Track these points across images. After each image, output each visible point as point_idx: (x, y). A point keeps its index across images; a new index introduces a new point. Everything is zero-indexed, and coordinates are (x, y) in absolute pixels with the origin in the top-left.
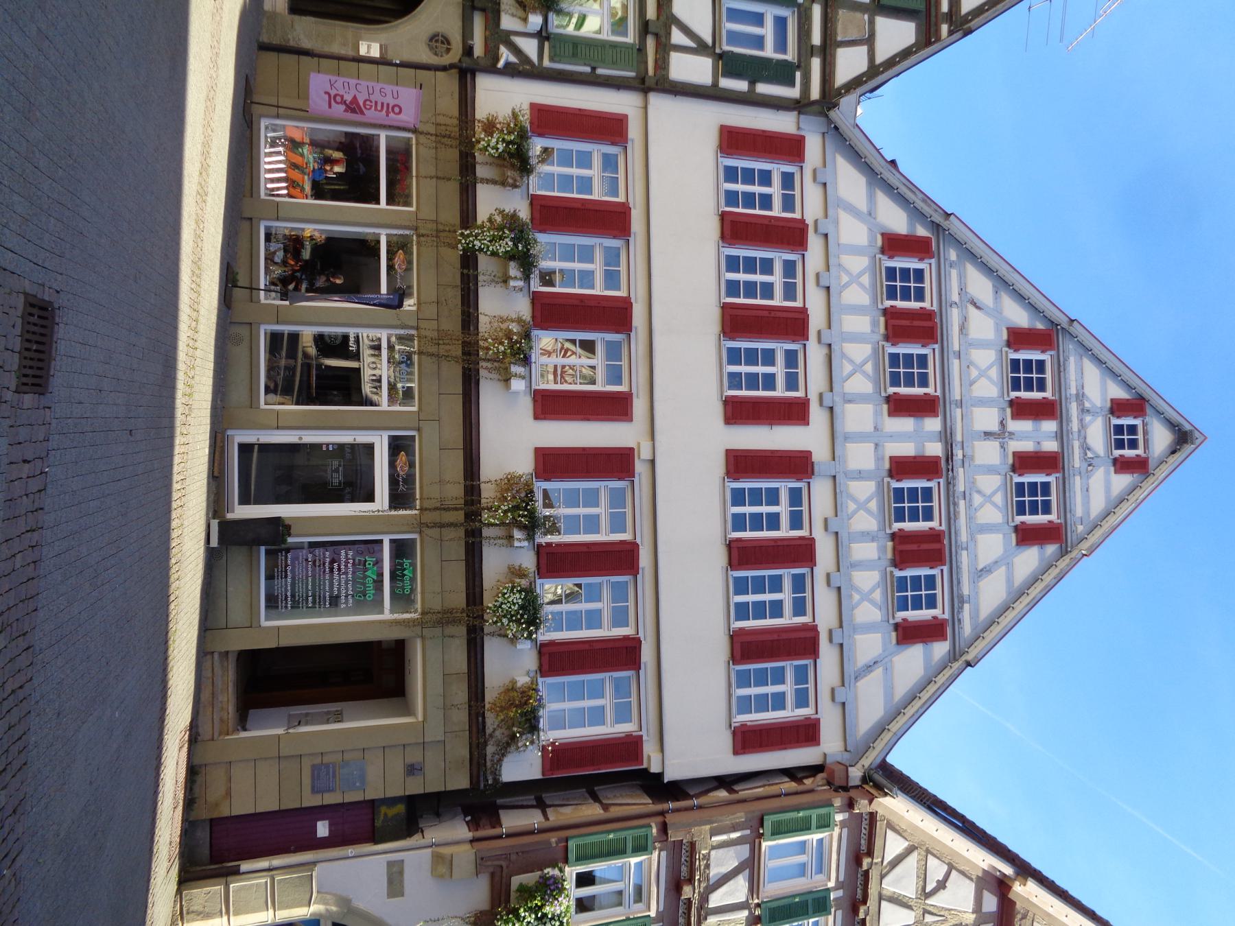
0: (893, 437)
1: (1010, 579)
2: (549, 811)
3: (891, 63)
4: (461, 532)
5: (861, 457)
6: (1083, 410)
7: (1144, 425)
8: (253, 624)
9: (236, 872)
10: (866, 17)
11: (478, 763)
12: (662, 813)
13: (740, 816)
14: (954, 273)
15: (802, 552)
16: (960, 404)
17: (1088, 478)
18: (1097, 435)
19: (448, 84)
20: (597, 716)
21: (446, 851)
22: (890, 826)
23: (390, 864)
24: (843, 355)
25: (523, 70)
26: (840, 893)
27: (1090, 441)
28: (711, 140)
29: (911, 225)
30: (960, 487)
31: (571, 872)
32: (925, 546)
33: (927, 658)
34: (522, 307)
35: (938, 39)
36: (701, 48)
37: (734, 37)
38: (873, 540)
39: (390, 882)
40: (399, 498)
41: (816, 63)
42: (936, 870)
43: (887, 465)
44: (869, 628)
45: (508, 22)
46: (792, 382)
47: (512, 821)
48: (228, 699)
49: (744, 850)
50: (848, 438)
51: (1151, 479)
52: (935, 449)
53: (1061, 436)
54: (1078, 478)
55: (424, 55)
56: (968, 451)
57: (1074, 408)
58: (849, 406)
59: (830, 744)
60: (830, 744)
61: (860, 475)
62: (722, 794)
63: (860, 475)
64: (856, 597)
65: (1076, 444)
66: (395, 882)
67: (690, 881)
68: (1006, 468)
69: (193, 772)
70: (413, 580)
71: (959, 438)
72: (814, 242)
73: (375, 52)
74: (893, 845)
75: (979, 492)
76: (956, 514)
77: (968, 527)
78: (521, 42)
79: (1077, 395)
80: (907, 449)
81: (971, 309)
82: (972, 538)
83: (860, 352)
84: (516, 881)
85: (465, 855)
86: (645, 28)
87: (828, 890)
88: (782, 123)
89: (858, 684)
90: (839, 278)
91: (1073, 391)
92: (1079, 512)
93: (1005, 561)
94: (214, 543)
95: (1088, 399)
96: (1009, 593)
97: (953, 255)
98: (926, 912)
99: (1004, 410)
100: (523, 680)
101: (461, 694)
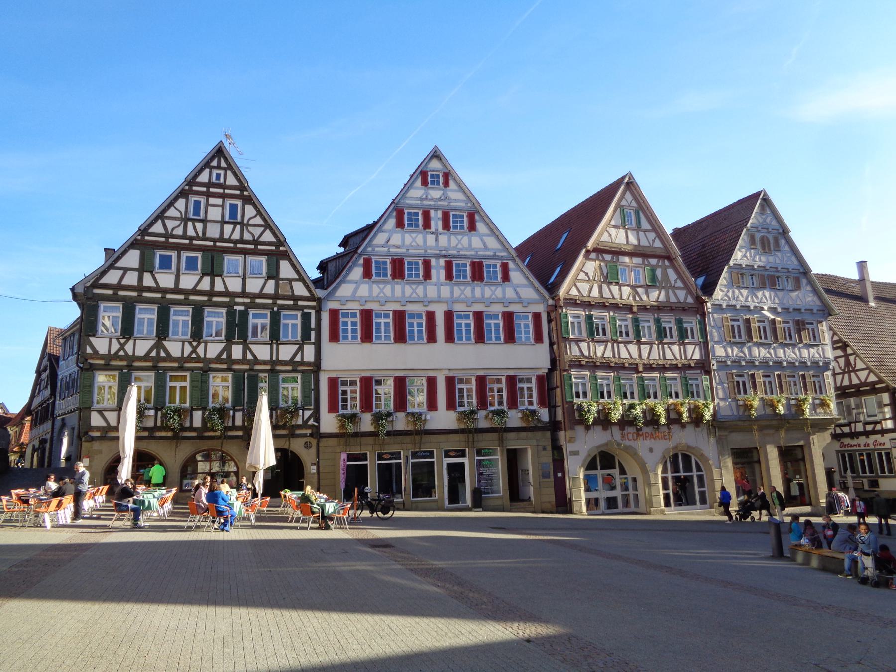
0: (438, 278)
1: (488, 236)
2: (557, 405)
3: (298, 272)
4: (475, 434)
5: (445, 291)
6: (426, 199)
7: (430, 171)
8: (502, 498)
9: (570, 499)
10: (280, 282)
11: (543, 428)
12: (560, 370)
13: (563, 345)
14: (377, 249)
15: (479, 316)
16: (426, 251)
17: (451, 199)
18: (435, 193)
19: (324, 442)
20: (527, 326)
21: (568, 438)
22: (568, 293)
23: (571, 455)
24: (410, 297)
25: (316, 415)
26: (587, 310)
27: (438, 197)
28: (334, 345)
29: (359, 266)
30: (455, 253)
31: (576, 400)
32: (477, 270)
33: (514, 270)
34: (401, 415)
35: (287, 251)
36: (301, 349)
37: (294, 334)
38: (474, 289)
39: (575, 455)
40: (462, 454)
41: (300, 303)
42: (582, 276)
43: (448, 281)
44: (504, 292)
45: (300, 422)
46: (419, 316)
47: (560, 416)
48: (522, 504)
49: (573, 344)
50: (439, 296)
51: (451, 172)
52: (442, 262)
53: (436, 209)
54: (452, 204)
55: (313, 450)
56: (443, 249)
57: (426, 202)
58: (428, 296)
59: (540, 308)
60: (540, 308)
61: (452, 292)
62: (555, 347)
63: (452, 292)
64: (494, 296)
65: (439, 203)
66: (575, 453)
67: (580, 362)
68: (448, 233)
69: (543, 512)
70: (488, 449)
71: (438, 252)
72: (369, 306)
73: (315, 467)
74: (574, 292)
75: (457, 245)
76: (465, 255)
77: (470, 251)
78: (306, 417)
79: (421, 200)
80: (442, 273)
81: (390, 243)
82: (473, 250)
83: (408, 290)
84: (577, 417)
85: (570, 433)
86: (294, 371)
87: (586, 315)
88: (325, 317)
89: (522, 297)
90: (382, 297)
91: (419, 202)
92: (463, 204)
93: (481, 237)
94: (481, 509)
95: (422, 196)
96: (492, 236)
97: (370, 249)
98: (594, 280)
99: (427, 232)
100: (520, 415)
101: (523, 434)
